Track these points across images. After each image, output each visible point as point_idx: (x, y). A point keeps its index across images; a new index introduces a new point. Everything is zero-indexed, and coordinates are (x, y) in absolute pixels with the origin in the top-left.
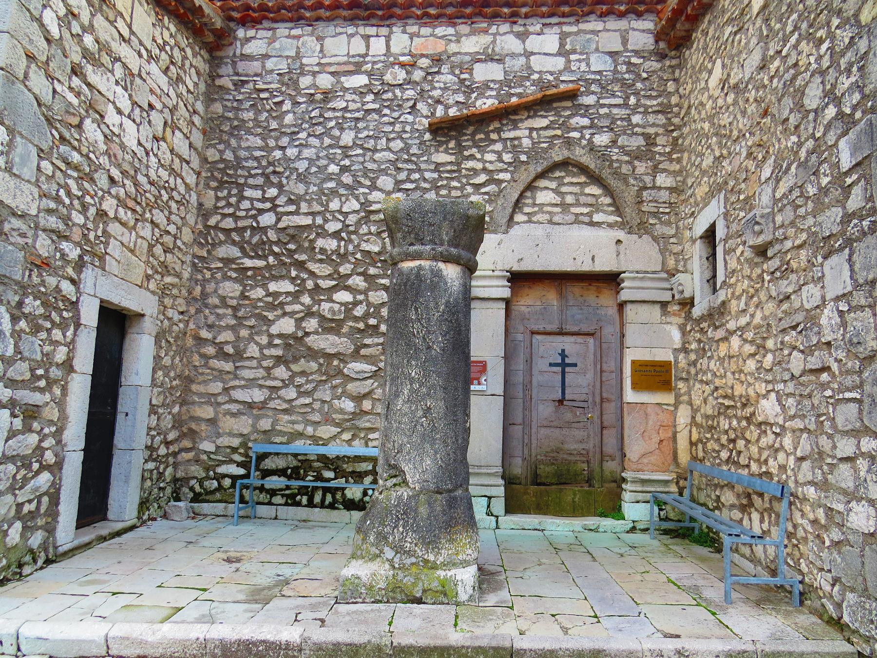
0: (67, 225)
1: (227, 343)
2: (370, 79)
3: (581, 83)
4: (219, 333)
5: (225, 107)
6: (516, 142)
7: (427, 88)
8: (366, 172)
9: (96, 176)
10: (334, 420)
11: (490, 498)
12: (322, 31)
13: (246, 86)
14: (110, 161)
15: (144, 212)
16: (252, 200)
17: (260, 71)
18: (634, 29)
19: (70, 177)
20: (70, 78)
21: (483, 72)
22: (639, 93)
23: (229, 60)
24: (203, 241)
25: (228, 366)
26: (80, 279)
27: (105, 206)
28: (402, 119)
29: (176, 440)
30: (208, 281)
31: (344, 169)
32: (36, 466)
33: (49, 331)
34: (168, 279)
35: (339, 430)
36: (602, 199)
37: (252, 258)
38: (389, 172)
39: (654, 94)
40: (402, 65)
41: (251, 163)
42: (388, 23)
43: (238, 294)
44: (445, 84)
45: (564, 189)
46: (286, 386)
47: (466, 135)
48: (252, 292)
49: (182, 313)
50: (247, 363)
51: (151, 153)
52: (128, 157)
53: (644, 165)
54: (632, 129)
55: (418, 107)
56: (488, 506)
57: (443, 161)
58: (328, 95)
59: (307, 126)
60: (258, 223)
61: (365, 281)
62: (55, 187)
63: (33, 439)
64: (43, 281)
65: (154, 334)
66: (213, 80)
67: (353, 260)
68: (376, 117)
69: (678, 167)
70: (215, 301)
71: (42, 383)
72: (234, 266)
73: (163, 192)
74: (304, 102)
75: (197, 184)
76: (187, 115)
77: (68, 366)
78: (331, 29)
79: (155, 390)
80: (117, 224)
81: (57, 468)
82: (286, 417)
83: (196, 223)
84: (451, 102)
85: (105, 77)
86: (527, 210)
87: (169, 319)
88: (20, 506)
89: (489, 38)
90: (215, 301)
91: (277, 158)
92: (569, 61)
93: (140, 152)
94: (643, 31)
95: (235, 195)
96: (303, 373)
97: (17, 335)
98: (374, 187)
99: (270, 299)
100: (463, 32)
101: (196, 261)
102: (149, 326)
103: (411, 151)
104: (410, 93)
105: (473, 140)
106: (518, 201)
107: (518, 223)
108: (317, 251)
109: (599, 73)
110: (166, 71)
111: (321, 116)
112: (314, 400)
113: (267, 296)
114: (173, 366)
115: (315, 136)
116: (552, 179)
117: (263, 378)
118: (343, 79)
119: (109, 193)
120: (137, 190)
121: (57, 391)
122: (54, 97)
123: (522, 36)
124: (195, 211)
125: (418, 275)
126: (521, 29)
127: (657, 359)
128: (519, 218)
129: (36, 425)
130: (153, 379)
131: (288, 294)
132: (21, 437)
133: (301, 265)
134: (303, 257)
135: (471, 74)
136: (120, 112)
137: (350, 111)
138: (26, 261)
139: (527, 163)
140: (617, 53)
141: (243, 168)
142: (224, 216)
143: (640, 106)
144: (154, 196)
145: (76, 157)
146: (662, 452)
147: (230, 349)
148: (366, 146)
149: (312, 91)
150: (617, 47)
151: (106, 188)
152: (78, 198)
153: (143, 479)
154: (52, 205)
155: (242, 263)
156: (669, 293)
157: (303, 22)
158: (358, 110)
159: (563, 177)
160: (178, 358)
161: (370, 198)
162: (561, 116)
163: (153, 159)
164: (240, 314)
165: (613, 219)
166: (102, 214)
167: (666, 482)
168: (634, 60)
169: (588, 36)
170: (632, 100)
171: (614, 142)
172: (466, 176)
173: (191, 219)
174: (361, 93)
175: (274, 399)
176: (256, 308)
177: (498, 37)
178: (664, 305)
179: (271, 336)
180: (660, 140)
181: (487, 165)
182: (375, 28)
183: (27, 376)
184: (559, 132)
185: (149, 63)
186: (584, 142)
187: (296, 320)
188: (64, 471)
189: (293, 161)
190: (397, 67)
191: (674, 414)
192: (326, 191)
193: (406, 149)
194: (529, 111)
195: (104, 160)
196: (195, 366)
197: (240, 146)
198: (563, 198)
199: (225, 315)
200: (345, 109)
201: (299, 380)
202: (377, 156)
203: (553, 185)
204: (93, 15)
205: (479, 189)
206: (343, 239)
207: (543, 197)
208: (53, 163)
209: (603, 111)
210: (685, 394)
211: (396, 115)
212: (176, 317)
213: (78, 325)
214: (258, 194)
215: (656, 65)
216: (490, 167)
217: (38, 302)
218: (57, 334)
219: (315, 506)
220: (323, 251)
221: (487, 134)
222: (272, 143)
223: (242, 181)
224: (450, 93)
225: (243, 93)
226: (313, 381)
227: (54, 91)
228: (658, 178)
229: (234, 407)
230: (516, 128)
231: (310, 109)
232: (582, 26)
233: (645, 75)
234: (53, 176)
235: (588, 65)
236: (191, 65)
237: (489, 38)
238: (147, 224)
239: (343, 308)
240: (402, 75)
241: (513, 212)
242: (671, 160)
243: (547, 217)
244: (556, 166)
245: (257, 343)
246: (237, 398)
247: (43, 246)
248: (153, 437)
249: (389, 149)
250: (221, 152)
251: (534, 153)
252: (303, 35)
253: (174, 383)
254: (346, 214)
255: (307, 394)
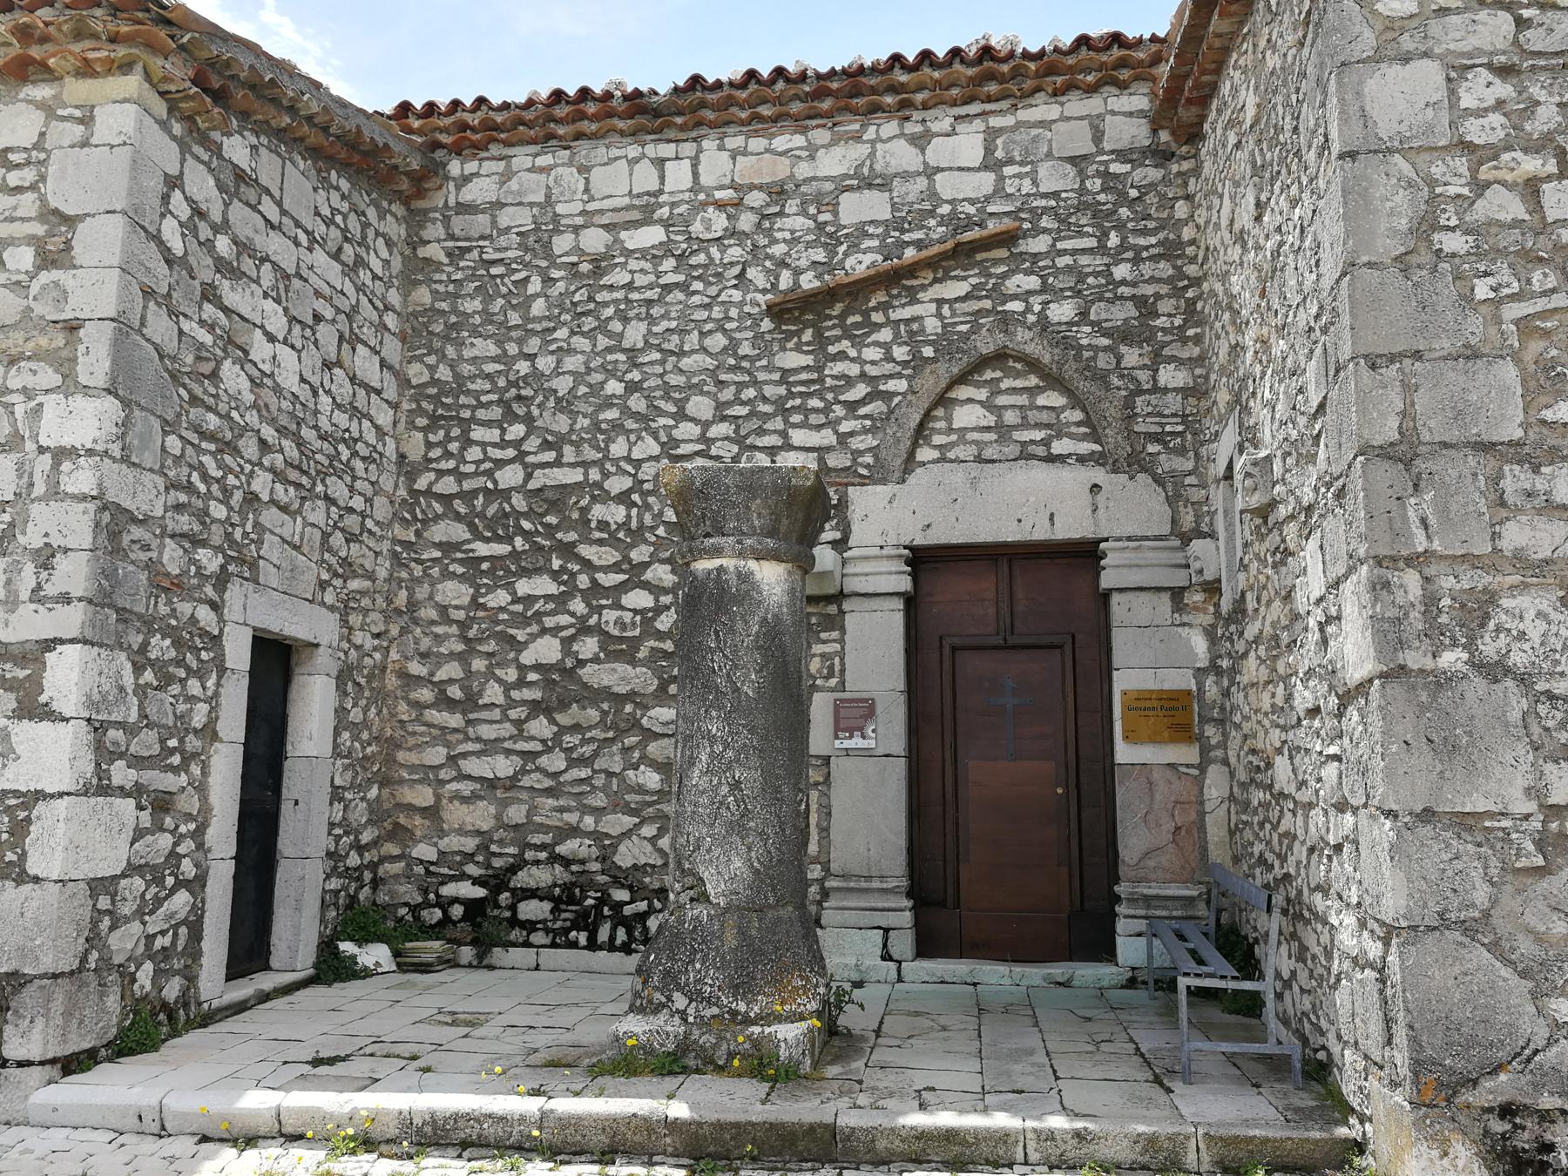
0: (203, 523)
1: (451, 681)
2: (667, 232)
3: (1023, 216)
4: (439, 665)
5: (435, 293)
6: (915, 326)
7: (763, 241)
8: (667, 389)
9: (241, 443)
10: (627, 804)
11: (886, 930)
12: (586, 157)
13: (467, 256)
14: (260, 416)
15: (314, 484)
16: (483, 445)
17: (488, 231)
18: (1113, 113)
19: (206, 452)
20: (200, 308)
21: (859, 208)
22: (1125, 226)
23: (437, 215)
24: (407, 516)
25: (455, 720)
26: (223, 601)
27: (256, 486)
28: (723, 298)
29: (375, 843)
30: (419, 581)
31: (632, 387)
32: (170, 881)
33: (183, 681)
34: (354, 584)
35: (637, 820)
36: (1067, 413)
37: (487, 540)
38: (706, 388)
39: (1151, 225)
40: (720, 206)
41: (480, 385)
42: (694, 134)
43: (466, 600)
44: (792, 232)
45: (1002, 400)
46: (549, 750)
47: (830, 318)
48: (490, 596)
49: (377, 636)
50: (484, 715)
51: (321, 391)
52: (285, 405)
53: (1137, 351)
54: (1114, 291)
55: (748, 276)
56: (885, 946)
57: (794, 366)
58: (600, 264)
59: (568, 317)
60: (495, 482)
61: (673, 572)
62: (186, 471)
63: (165, 841)
64: (174, 610)
65: (334, 673)
66: (415, 249)
67: (653, 539)
68: (681, 296)
69: (1196, 351)
70: (432, 614)
71: (176, 760)
72: (459, 555)
73: (341, 447)
74: (562, 278)
75: (395, 423)
76: (375, 316)
77: (209, 732)
78: (601, 152)
79: (339, 763)
80: (274, 510)
81: (197, 885)
82: (551, 802)
83: (396, 486)
84: (803, 263)
85: (248, 292)
86: (938, 440)
87: (358, 648)
88: (150, 938)
89: (865, 149)
90: (432, 614)
91: (522, 373)
92: (1001, 179)
93: (304, 393)
94: (1130, 114)
95: (456, 439)
96: (576, 728)
97: (141, 691)
98: (681, 416)
99: (519, 608)
100: (819, 142)
101: (399, 549)
102: (325, 660)
103: (741, 352)
104: (735, 253)
105: (842, 325)
106: (921, 425)
107: (924, 464)
108: (593, 525)
109: (1055, 195)
110: (336, 256)
111: (591, 299)
112: (594, 771)
113: (513, 602)
114: (366, 724)
115: (583, 334)
116: (978, 385)
117: (511, 738)
118: (623, 235)
119: (260, 464)
120: (302, 453)
121: (196, 770)
122: (180, 341)
123: (920, 141)
124: (393, 468)
125: (718, 580)
126: (919, 128)
127: (1166, 686)
128: (925, 454)
129: (169, 822)
130: (336, 746)
131: (548, 598)
132: (149, 838)
133: (568, 550)
134: (572, 536)
135: (836, 213)
136: (271, 338)
137: (638, 289)
138: (151, 585)
139: (934, 360)
140: (1084, 157)
141: (468, 392)
142: (441, 473)
143: (1127, 249)
144: (328, 456)
145: (212, 421)
146: (1181, 849)
147: (455, 692)
148: (665, 346)
149: (574, 259)
150: (1085, 146)
151: (255, 459)
152: (218, 481)
153: (324, 906)
154: (183, 498)
155: (472, 551)
156: (1183, 573)
157: (554, 142)
158: (650, 287)
159: (999, 380)
160: (373, 710)
161: (676, 433)
162: (990, 275)
163: (325, 400)
164: (471, 634)
165: (1086, 447)
166: (252, 499)
167: (1189, 901)
168: (1116, 168)
169: (1034, 132)
170: (1114, 240)
171: (1083, 315)
172: (832, 389)
173: (387, 483)
174: (654, 256)
175: (529, 772)
176: (498, 622)
177: (879, 146)
178: (1177, 594)
179: (522, 669)
180: (1165, 306)
181: (868, 368)
182: (673, 145)
183: (156, 749)
184: (987, 304)
185: (310, 249)
186: (1031, 318)
187: (563, 640)
188: (208, 889)
189: (549, 378)
190: (711, 209)
191: (1199, 782)
192: (603, 426)
193: (732, 347)
194: (935, 271)
195: (252, 418)
196: (401, 721)
197: (461, 357)
198: (1000, 417)
199: (447, 636)
200: (630, 286)
201: (570, 740)
202: (686, 363)
203: (982, 394)
204: (226, 205)
205: (855, 410)
206: (634, 504)
207: (966, 416)
208: (181, 437)
209: (1062, 262)
210: (1218, 746)
211: (713, 291)
212: (369, 643)
213: (222, 670)
214: (493, 435)
215: (1154, 174)
216: (872, 371)
217: (168, 642)
218: (194, 687)
219: (601, 948)
220: (603, 525)
221: (866, 314)
222: (512, 349)
223: (466, 414)
224: (801, 247)
225: (463, 269)
226: (592, 740)
227: (181, 332)
228: (1162, 371)
229: (466, 788)
230: (914, 301)
231: (572, 288)
232: (1023, 115)
233: (1134, 193)
234: (182, 455)
235: (1035, 182)
236: (377, 234)
237: (865, 149)
238: (319, 503)
239: (638, 618)
240: (720, 222)
241: (915, 445)
242: (1184, 340)
243: (973, 450)
244: (983, 362)
245: (500, 681)
246: (469, 771)
247: (172, 557)
248: (338, 838)
249: (704, 350)
250: (432, 369)
251: (947, 343)
252: (556, 166)
253: (369, 750)
254: (638, 464)
255: (584, 761)
